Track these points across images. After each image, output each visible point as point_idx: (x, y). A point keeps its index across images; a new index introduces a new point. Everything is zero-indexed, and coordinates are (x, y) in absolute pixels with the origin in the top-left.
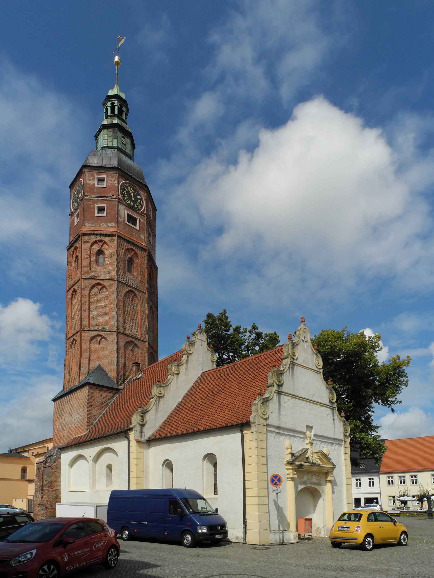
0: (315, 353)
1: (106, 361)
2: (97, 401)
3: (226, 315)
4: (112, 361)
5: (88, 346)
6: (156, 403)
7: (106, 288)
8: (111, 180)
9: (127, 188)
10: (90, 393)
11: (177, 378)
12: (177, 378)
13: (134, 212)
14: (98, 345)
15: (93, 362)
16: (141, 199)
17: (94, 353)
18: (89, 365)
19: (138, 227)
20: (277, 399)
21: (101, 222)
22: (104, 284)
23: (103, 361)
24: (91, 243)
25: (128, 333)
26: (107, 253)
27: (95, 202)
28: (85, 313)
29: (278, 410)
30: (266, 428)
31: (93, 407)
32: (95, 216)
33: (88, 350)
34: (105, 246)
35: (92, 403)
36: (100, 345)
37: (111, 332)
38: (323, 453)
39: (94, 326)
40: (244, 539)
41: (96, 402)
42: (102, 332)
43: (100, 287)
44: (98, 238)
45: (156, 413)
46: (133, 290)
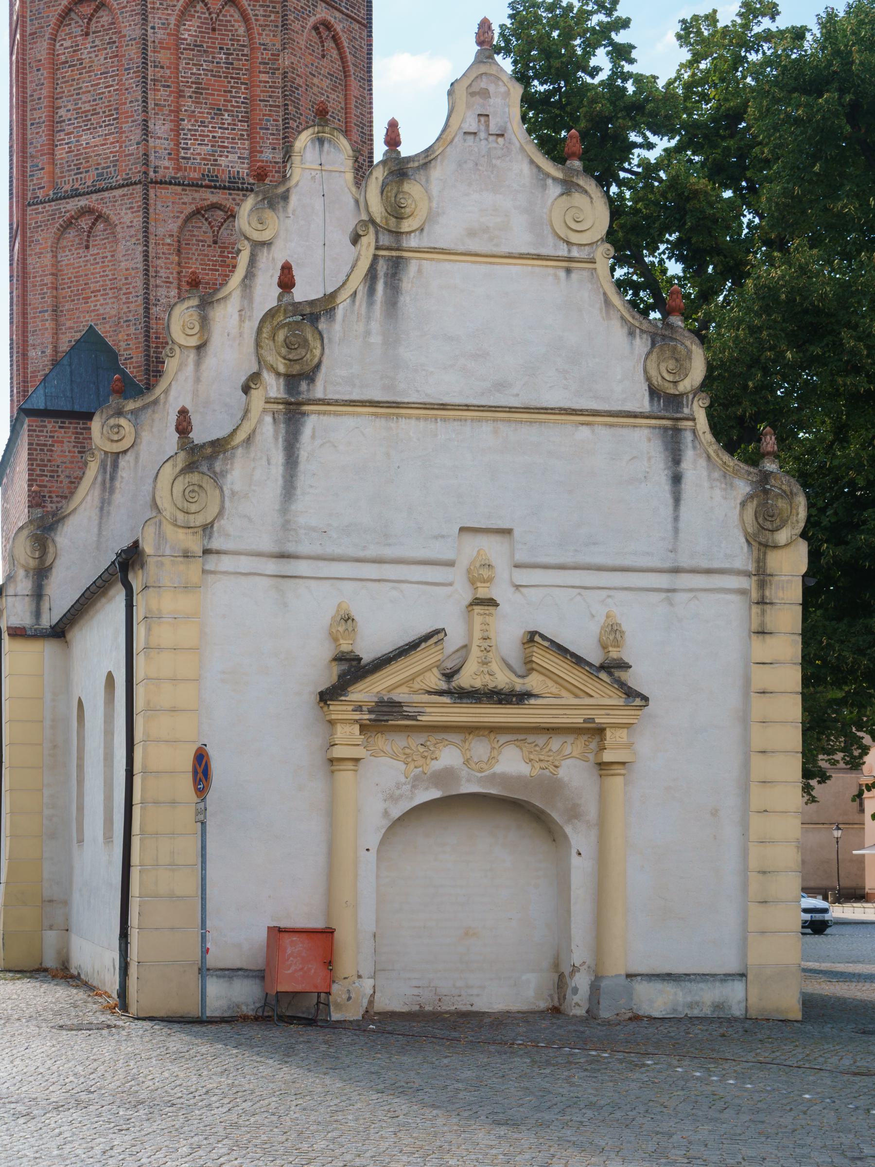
0: (555, 179)
2: (69, 477)
4: (132, 306)
10: (38, 448)
11: (198, 364)
12: (198, 364)
15: (70, 320)
17: (69, 287)
23: (102, 311)
25: (196, 175)
28: (37, 133)
29: (280, 481)
31: (51, 502)
35: (45, 486)
36: (92, 251)
37: (126, 189)
39: (71, 178)
41: (61, 482)
42: (94, 197)
45: (101, 517)
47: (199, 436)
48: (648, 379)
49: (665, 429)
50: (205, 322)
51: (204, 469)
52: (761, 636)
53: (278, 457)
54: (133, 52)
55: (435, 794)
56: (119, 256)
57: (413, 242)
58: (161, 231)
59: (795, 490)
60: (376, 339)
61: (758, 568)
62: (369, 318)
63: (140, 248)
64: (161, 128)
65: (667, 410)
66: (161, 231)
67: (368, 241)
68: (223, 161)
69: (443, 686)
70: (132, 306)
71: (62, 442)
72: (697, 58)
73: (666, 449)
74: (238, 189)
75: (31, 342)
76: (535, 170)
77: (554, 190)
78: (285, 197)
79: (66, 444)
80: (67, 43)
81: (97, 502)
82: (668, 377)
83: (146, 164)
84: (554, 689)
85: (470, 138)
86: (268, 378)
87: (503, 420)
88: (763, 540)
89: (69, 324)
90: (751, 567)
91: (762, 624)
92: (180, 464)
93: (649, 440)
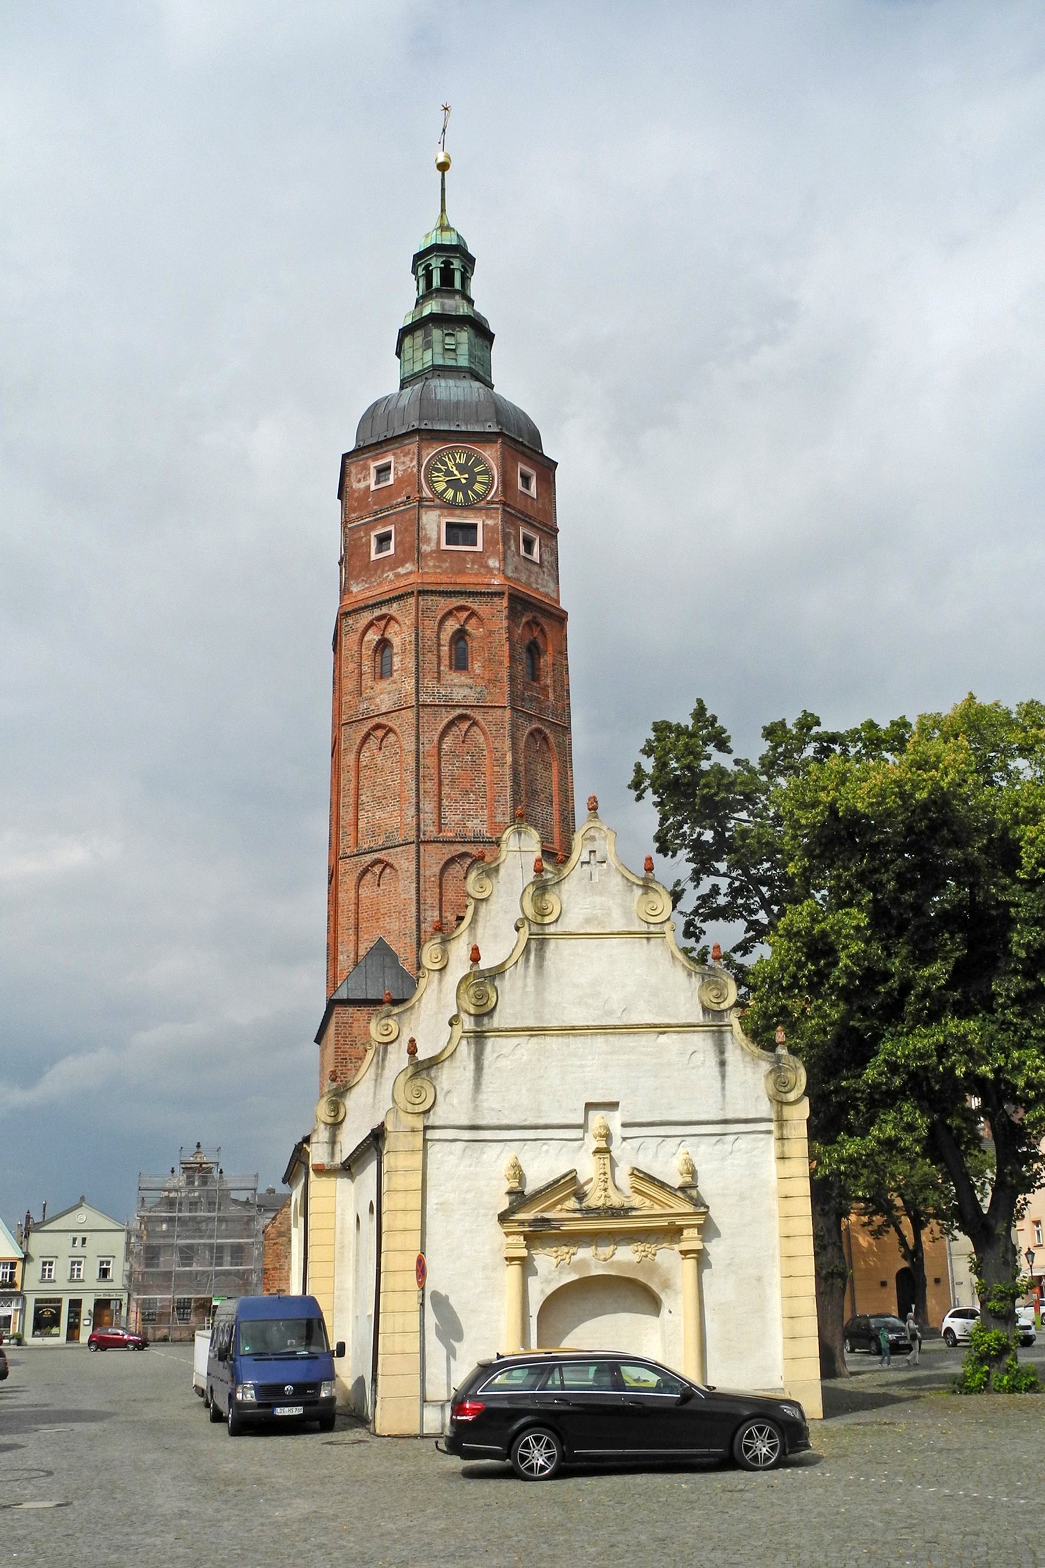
0: (638, 885)
1: (395, 926)
3: (708, 714)
4: (408, 925)
5: (353, 899)
6: (375, 1061)
7: (395, 733)
8: (403, 463)
9: (445, 464)
11: (440, 981)
12: (440, 981)
13: (465, 513)
14: (375, 888)
16: (487, 472)
18: (357, 944)
19: (479, 547)
21: (383, 572)
22: (390, 724)
24: (360, 630)
25: (451, 834)
26: (396, 641)
27: (369, 527)
29: (472, 1081)
30: (424, 1135)
32: (369, 562)
33: (352, 907)
34: (393, 628)
35: (347, 1052)
36: (382, 887)
38: (641, 1175)
43: (380, 733)
44: (377, 613)
45: (376, 1086)
46: (466, 715)
47: (422, 1055)
48: (702, 1002)
50: (445, 953)
51: (425, 1076)
52: (782, 1161)
53: (471, 1066)
54: (411, 760)
55: (574, 1277)
56: (399, 890)
57: (552, 929)
58: (428, 873)
59: (798, 1065)
60: (530, 988)
61: (778, 1117)
62: (525, 977)
63: (414, 885)
65: (714, 1021)
66: (428, 873)
67: (525, 932)
68: (469, 824)
69: (578, 1206)
70: (408, 925)
71: (359, 1020)
72: (774, 748)
73: (715, 1045)
74: (480, 842)
75: (340, 950)
76: (625, 881)
77: (638, 892)
78: (497, 870)
79: (361, 1021)
80: (366, 755)
81: (373, 1077)
82: (715, 1000)
83: (418, 830)
84: (648, 1203)
85: (585, 866)
86: (464, 1016)
87: (611, 1033)
88: (780, 1099)
89: (366, 937)
90: (773, 1116)
91: (783, 1152)
92: (410, 1073)
93: (704, 1040)
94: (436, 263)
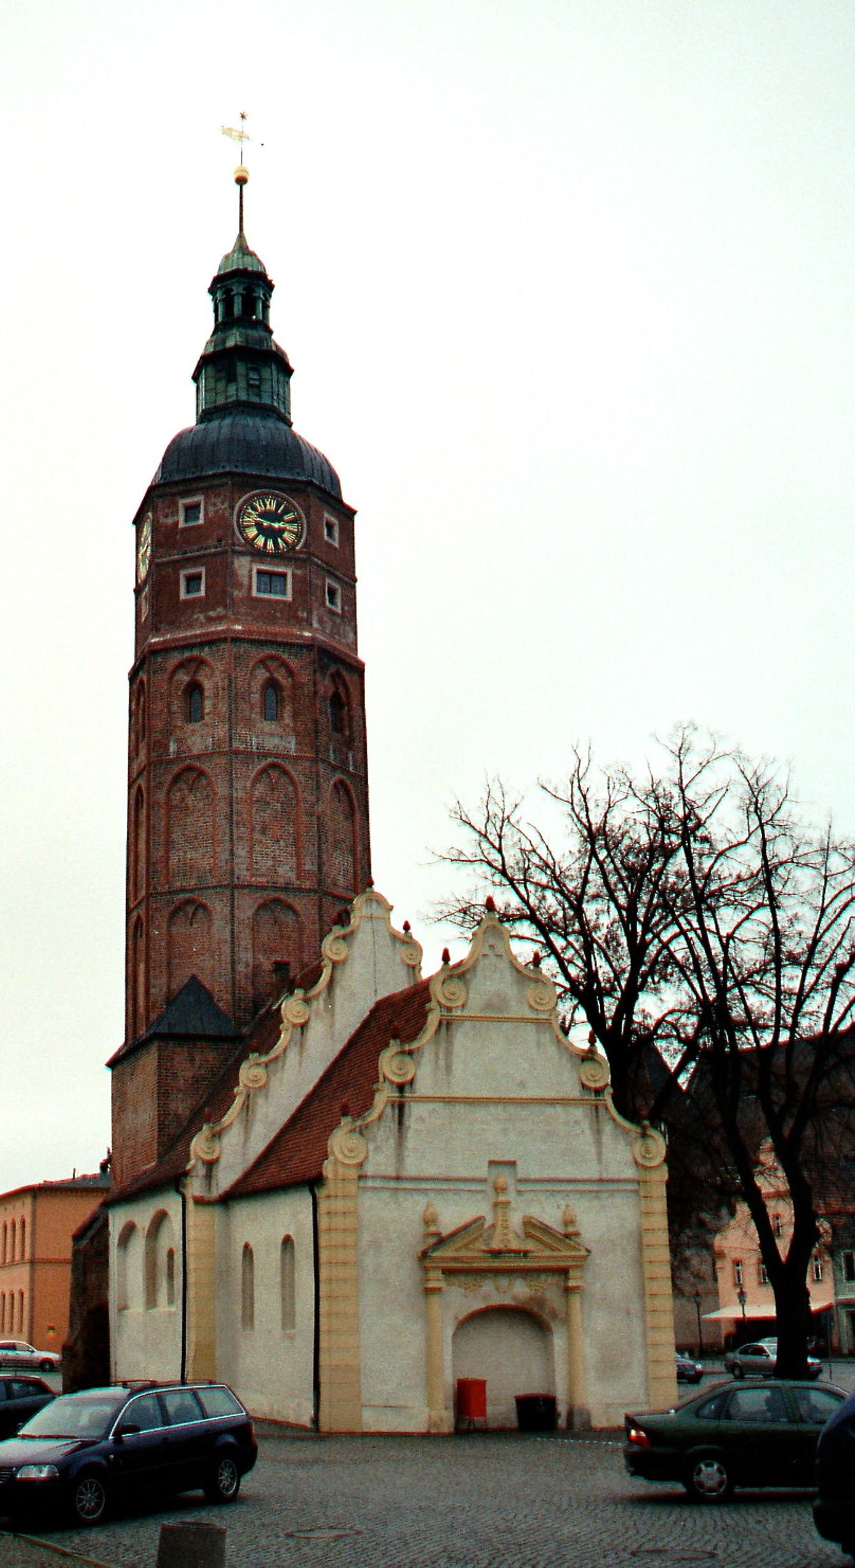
20: (393, 1116)
21: (193, 613)
23: (201, 965)
25: (265, 880)
26: (207, 684)
27: (177, 565)
36: (195, 926)
40: (316, 1420)
44: (187, 654)
49: (592, 1105)
64: (241, 851)
66: (242, 916)
68: (280, 870)
76: (515, 974)
94: (238, 289)
